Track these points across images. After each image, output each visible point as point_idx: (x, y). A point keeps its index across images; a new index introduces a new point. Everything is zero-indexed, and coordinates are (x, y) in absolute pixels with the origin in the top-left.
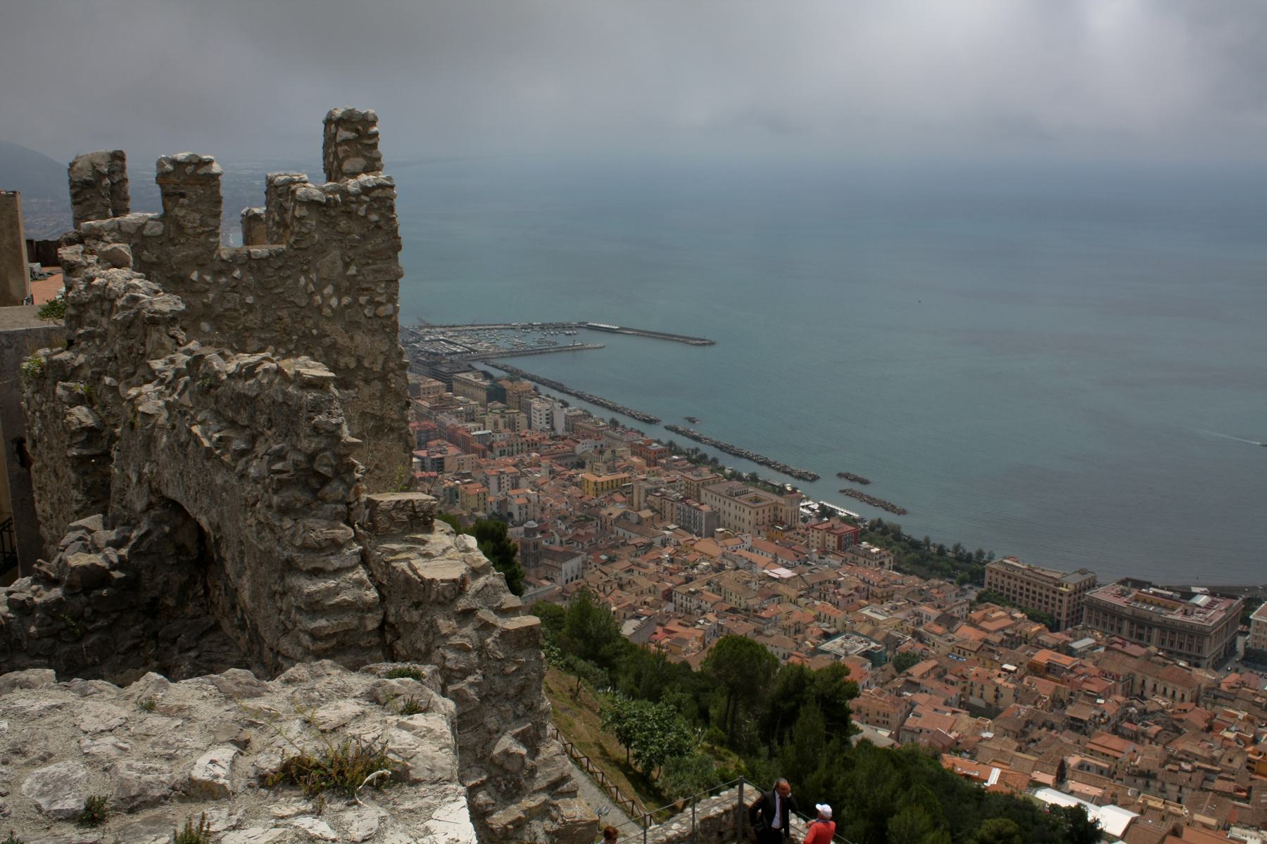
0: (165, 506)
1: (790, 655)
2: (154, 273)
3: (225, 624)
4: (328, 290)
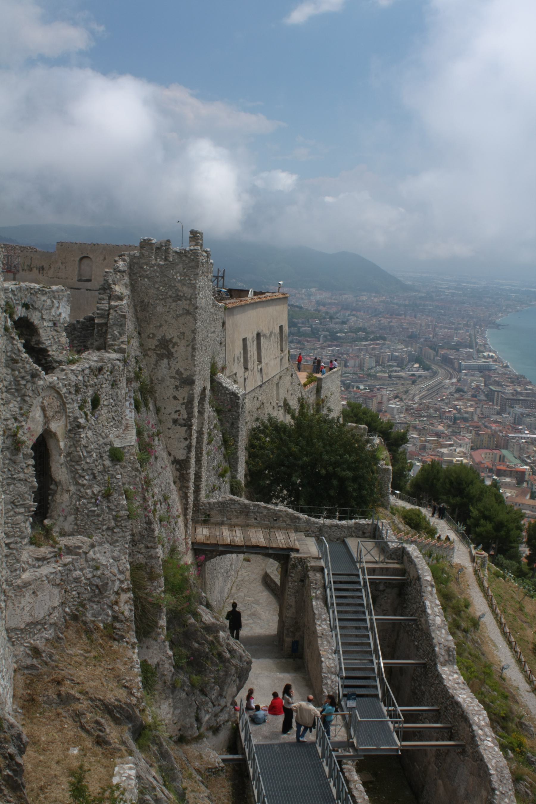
4: (178, 275)
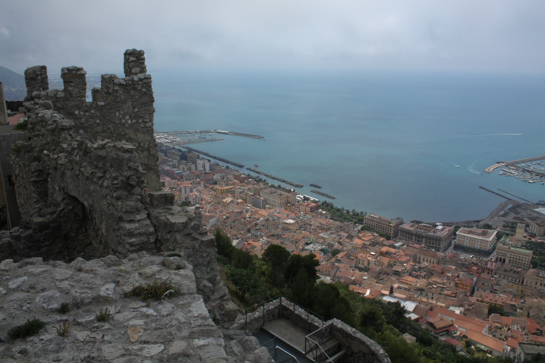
0: (69, 199)
1: (294, 251)
2: (61, 111)
3: (94, 242)
4: (127, 117)
